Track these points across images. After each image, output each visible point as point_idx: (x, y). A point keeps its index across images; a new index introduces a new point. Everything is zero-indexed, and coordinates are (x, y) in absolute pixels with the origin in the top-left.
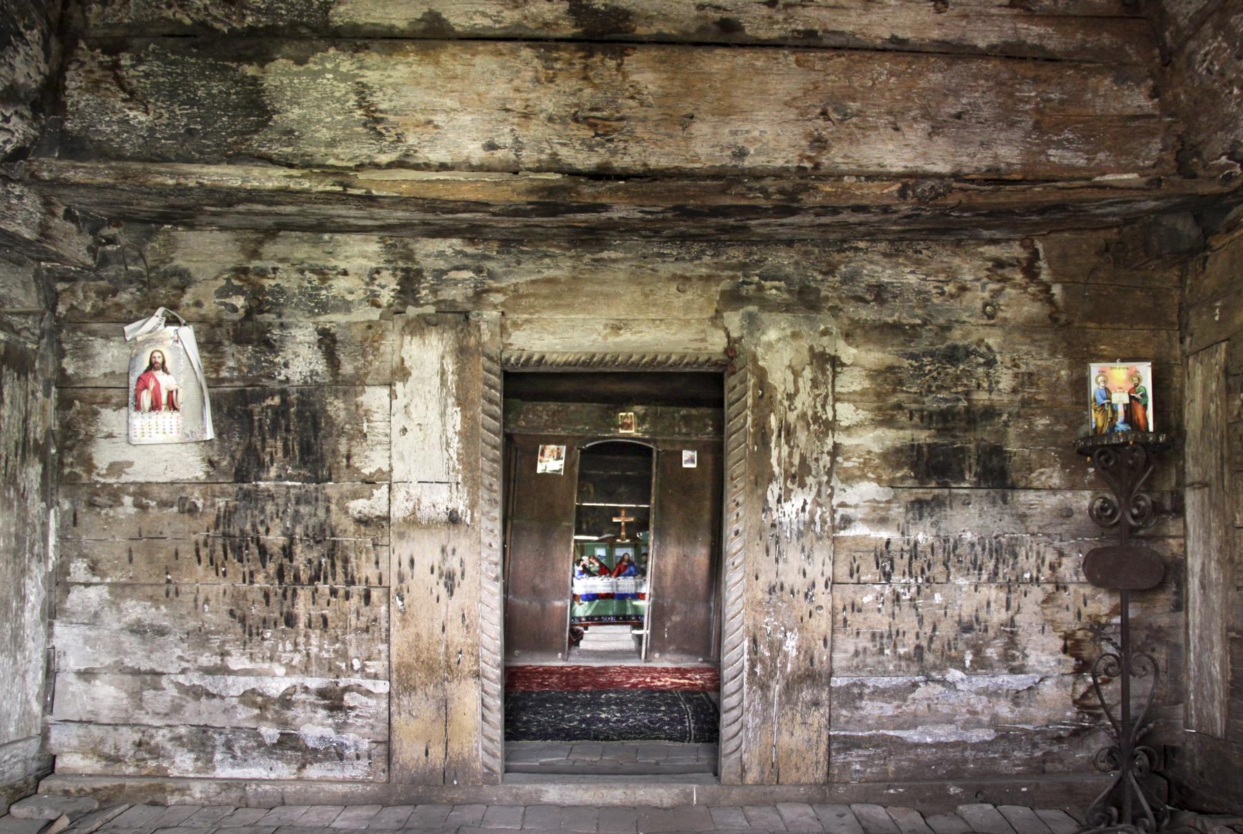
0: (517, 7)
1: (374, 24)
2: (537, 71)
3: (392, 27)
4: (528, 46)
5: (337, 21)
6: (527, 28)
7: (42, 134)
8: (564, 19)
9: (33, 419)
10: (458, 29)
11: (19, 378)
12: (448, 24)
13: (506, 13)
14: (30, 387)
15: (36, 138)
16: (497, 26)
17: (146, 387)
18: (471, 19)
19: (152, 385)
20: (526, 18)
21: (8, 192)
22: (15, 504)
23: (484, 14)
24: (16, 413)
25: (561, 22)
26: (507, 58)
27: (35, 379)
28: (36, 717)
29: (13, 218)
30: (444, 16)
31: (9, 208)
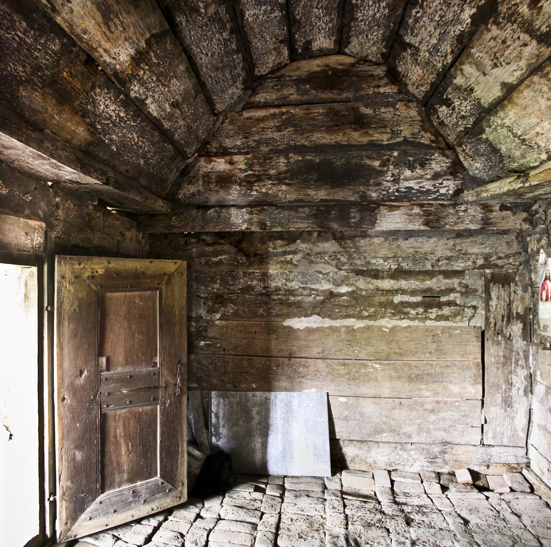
0: (521, 58)
1: (494, 100)
2: (547, 85)
3: (499, 97)
4: (534, 75)
5: (486, 105)
6: (533, 63)
7: (464, 180)
8: (541, 48)
9: (515, 303)
10: (515, 83)
11: (503, 287)
12: (510, 83)
13: (521, 64)
14: (512, 289)
15: (462, 183)
16: (524, 71)
17: (544, 289)
18: (514, 76)
19: (546, 288)
20: (528, 60)
21: (457, 211)
22: (503, 342)
23: (515, 71)
24: (502, 302)
25: (541, 50)
26: (532, 86)
27: (516, 285)
28: (522, 439)
29: (462, 222)
30: (506, 81)
31: (458, 219)
